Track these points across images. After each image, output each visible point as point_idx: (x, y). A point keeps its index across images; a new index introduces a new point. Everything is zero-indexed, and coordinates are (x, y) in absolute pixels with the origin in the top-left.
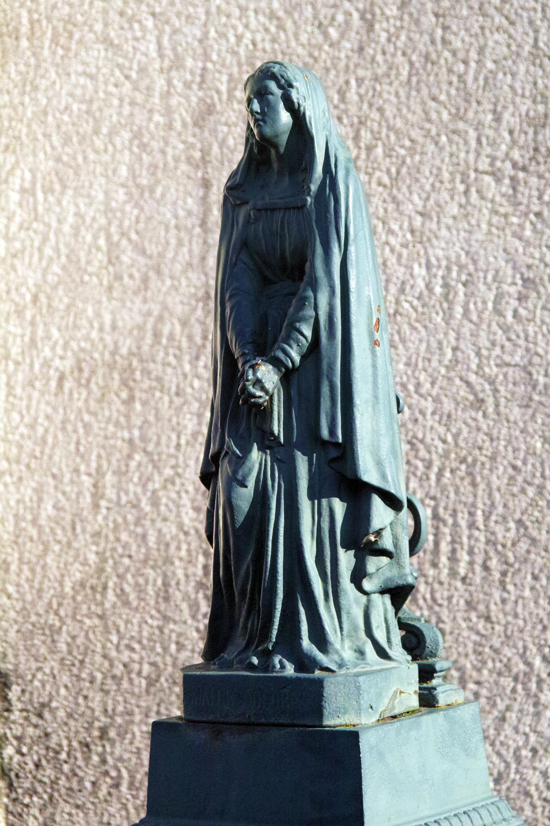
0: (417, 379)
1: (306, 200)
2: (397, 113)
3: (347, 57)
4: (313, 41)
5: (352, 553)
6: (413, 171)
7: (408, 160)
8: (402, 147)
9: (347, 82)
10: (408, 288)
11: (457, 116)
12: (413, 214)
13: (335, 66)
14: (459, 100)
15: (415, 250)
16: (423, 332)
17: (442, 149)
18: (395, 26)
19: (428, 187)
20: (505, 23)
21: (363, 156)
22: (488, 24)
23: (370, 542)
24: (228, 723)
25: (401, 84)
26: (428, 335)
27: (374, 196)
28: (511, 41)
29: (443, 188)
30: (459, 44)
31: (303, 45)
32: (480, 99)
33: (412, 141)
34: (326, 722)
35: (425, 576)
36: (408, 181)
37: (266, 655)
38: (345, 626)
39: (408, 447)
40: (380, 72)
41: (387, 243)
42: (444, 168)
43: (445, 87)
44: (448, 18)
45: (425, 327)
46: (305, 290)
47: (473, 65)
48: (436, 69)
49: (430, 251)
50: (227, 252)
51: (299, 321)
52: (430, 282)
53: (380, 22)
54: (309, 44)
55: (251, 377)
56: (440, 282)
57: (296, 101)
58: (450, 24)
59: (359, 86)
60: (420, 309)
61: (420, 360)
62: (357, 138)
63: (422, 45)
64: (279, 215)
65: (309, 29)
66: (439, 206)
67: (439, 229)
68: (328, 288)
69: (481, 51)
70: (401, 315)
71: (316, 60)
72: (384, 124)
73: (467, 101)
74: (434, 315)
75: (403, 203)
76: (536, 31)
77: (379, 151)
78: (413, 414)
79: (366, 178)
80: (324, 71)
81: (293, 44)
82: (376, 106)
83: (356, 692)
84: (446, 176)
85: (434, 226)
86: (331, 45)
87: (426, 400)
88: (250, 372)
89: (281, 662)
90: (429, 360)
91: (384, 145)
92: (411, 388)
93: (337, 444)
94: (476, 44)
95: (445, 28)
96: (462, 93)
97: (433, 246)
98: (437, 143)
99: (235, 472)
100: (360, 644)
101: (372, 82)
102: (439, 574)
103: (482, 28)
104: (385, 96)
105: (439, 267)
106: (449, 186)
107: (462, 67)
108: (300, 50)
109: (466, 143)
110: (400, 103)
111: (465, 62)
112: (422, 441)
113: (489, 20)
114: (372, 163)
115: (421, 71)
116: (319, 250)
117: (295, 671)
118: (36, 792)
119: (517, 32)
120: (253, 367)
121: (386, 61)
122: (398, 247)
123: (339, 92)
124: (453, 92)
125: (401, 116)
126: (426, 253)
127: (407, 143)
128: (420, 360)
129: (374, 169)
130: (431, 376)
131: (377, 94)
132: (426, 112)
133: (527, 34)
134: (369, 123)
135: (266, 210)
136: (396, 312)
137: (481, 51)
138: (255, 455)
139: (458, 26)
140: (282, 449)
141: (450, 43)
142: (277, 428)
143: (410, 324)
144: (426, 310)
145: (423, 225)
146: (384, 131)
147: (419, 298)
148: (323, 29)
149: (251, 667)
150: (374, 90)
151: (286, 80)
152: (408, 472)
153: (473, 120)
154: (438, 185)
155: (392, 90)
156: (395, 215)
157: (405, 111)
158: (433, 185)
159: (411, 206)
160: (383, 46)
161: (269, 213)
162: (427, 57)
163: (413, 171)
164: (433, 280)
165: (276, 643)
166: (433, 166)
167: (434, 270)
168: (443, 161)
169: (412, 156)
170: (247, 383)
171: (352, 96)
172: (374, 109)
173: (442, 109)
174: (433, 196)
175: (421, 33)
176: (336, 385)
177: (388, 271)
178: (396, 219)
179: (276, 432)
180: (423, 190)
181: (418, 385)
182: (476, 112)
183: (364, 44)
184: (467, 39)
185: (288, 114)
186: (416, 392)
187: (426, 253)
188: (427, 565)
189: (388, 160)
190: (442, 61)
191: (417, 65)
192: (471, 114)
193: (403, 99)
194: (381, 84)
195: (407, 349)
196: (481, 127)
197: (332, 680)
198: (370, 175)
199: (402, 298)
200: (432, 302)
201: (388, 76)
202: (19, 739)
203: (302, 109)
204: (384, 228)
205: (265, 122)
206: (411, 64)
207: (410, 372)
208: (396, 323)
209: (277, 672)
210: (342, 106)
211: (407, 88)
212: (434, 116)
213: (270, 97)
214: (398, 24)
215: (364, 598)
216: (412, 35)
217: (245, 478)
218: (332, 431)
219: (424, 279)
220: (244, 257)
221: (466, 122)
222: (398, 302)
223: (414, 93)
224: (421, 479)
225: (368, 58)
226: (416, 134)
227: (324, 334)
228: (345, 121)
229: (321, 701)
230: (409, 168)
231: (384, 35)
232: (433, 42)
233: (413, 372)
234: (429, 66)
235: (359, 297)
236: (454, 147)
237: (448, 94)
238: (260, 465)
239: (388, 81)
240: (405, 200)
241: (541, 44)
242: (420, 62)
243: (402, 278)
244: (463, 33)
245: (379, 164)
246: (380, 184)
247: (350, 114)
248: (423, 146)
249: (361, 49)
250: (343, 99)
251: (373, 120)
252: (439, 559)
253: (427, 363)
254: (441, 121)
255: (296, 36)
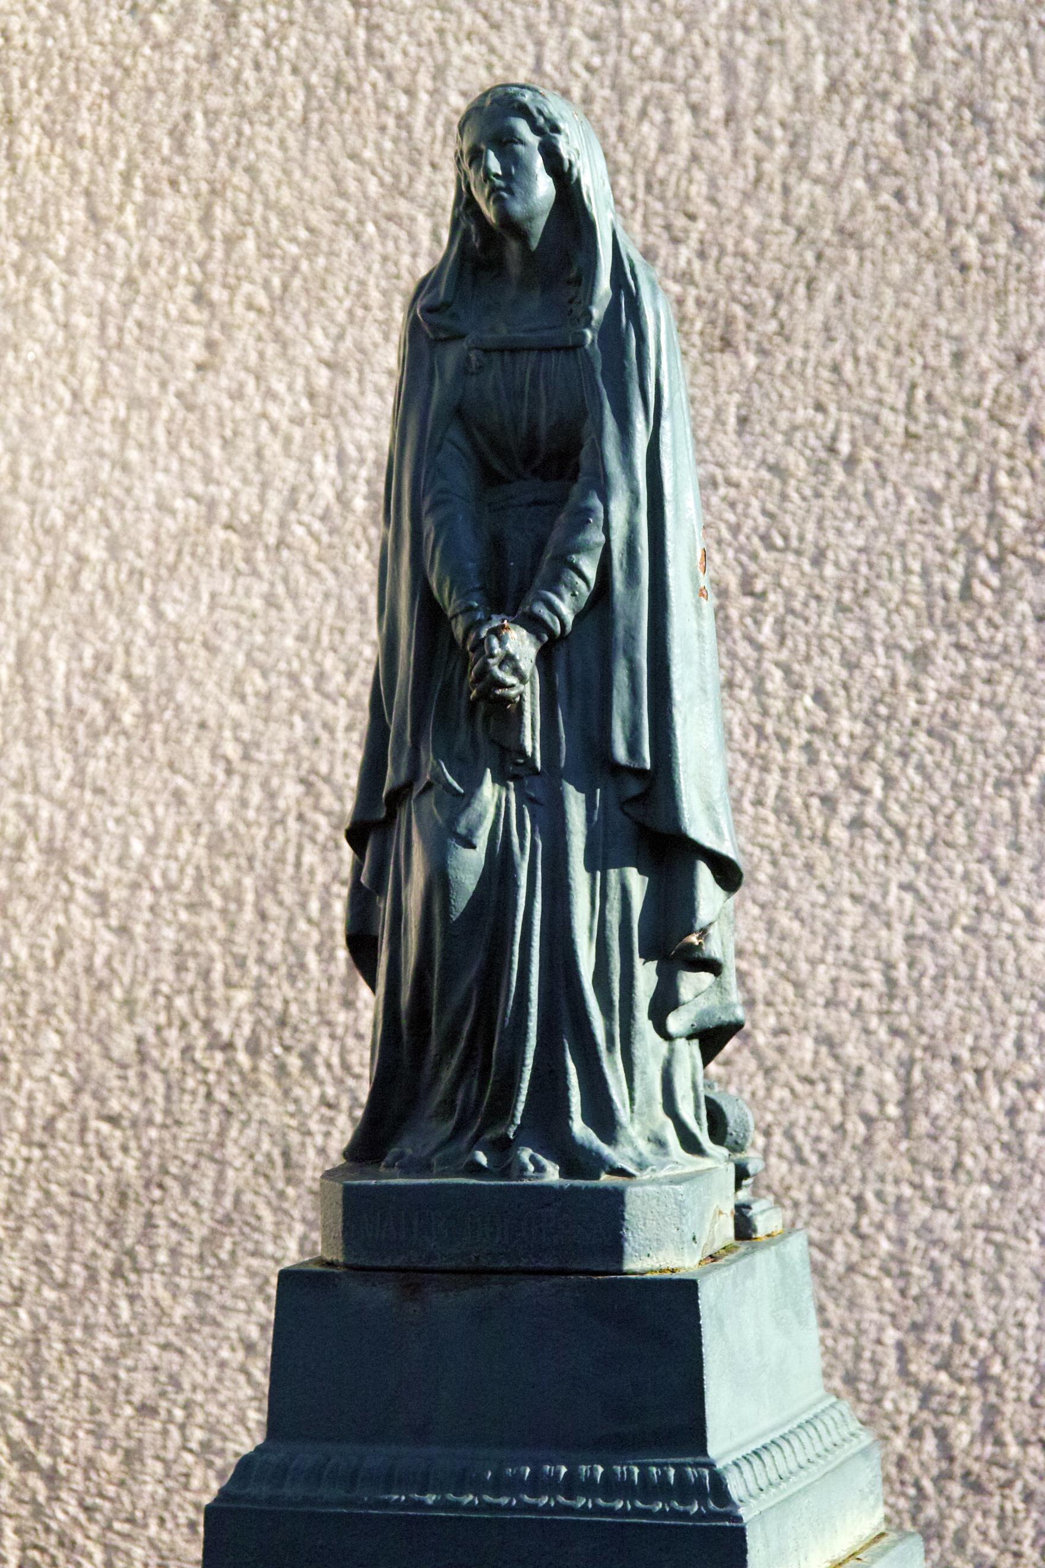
0: (319, 665)
1: (584, 336)
2: (284, 178)
3: (187, 70)
4: (123, 38)
5: (653, 965)
6: (314, 286)
7: (304, 265)
8: (293, 240)
9: (187, 117)
10: (303, 498)
11: (397, 190)
12: (313, 364)
13: (164, 86)
14: (398, 159)
15: (317, 429)
16: (331, 581)
17: (366, 248)
18: (278, 19)
19: (341, 317)
20: (483, 25)
21: (219, 253)
22: (451, 25)
23: (692, 945)
24: (433, 1271)
25: (289, 126)
26: (341, 587)
27: (239, 327)
28: (494, 59)
29: (370, 318)
30: (398, 59)
31: (101, 44)
32: (437, 160)
33: (310, 230)
35: (329, 1023)
36: (304, 304)
37: (503, 1148)
38: (638, 1095)
39: (300, 789)
40: (250, 100)
41: (264, 415)
42: (372, 282)
43: (372, 135)
44: (378, 10)
45: (335, 571)
46: (585, 496)
47: (424, 97)
48: (354, 101)
49: (346, 433)
50: (423, 423)
51: (578, 551)
52: (344, 489)
53: (250, 10)
54: (114, 43)
55: (497, 650)
56: (363, 489)
57: (565, 156)
58: (381, 20)
59: (210, 125)
60: (325, 538)
61: (325, 631)
62: (206, 220)
63: (329, 53)
64: (527, 362)
65: (114, 14)
66: (362, 351)
67: (362, 393)
68: (627, 494)
69: (439, 73)
70: (289, 547)
71: (127, 71)
72: (257, 196)
73: (414, 163)
74: (351, 549)
75: (294, 342)
76: (540, 43)
77: (249, 245)
78: (310, 728)
79: (225, 295)
80: (143, 94)
81: (83, 40)
82: (244, 162)
83: (677, 1213)
84: (375, 296)
85: (352, 387)
86: (156, 47)
87: (335, 703)
88: (495, 642)
89: (532, 1159)
90: (342, 632)
91: (258, 235)
92: (308, 681)
93: (641, 773)
94: (429, 61)
95: (372, 28)
96: (404, 148)
97: (349, 424)
98: (357, 237)
99: (452, 822)
100: (656, 1127)
101: (236, 119)
102: (356, 1020)
103: (441, 32)
104: (261, 145)
105: (362, 462)
106: (380, 316)
107: (404, 101)
108: (96, 52)
109: (412, 237)
110: (288, 160)
111: (410, 92)
112: (327, 779)
113: (453, 18)
114: (236, 267)
115: (328, 104)
116: (610, 425)
117: (564, 1174)
119: (504, 42)
120: (496, 632)
121: (261, 81)
122: (284, 424)
123: (171, 133)
124: (388, 145)
125: (290, 184)
126: (338, 435)
127: (303, 234)
128: (325, 631)
129: (239, 279)
130: (344, 660)
131: (244, 140)
132: (337, 180)
133: (522, 48)
134: (229, 194)
135: (501, 351)
136: (281, 543)
137: (439, 73)
138: (489, 791)
139: (396, 25)
140: (537, 780)
141: (382, 56)
142: (531, 742)
143: (306, 565)
144: (336, 540)
145: (332, 384)
146: (259, 210)
147: (323, 518)
148: (140, 16)
149: (476, 1169)
150: (240, 133)
151: (546, 120)
152: (300, 834)
153: (425, 198)
154: (359, 312)
155: (273, 135)
156: (281, 364)
157: (297, 175)
158: (350, 313)
159: (309, 350)
160: (256, 55)
161: (507, 357)
162: (338, 78)
163: (314, 286)
164: (351, 486)
165: (520, 1127)
166: (350, 278)
167: (353, 467)
168: (369, 270)
169: (310, 259)
170: (491, 661)
171: (197, 142)
172: (239, 169)
173: (367, 174)
174: (351, 332)
175: (327, 36)
176: (639, 667)
177: (266, 467)
178: (282, 373)
179: (529, 750)
180: (333, 321)
181: (321, 677)
182: (431, 184)
183: (219, 49)
184: (412, 50)
185: (550, 180)
186: (318, 689)
187: (338, 435)
188: (334, 1005)
189: (265, 263)
190: (367, 88)
191: (321, 92)
192: (420, 187)
193: (294, 151)
194: (251, 123)
195: (300, 611)
196: (438, 211)
197: (638, 1190)
198: (232, 289)
199: (293, 516)
200: (349, 526)
201: (266, 109)
203: (575, 171)
204: (258, 388)
205: (511, 192)
206: (309, 88)
207: (305, 653)
208: (280, 562)
209: (530, 1178)
210: (178, 160)
211: (301, 134)
212: (352, 186)
213: (520, 148)
214: (284, 15)
215: (663, 1046)
216: (310, 36)
217: (472, 831)
219: (333, 483)
220: (455, 433)
221: (412, 200)
222: (283, 524)
223: (314, 143)
224: (324, 848)
225: (228, 74)
226: (317, 217)
228: (184, 188)
229: (620, 1227)
230: (305, 280)
231: (257, 34)
232: (349, 52)
233: (312, 652)
234: (343, 95)
235: (677, 509)
236: (390, 244)
237: (379, 149)
238: (498, 807)
239: (265, 118)
240: (299, 339)
241: (548, 68)
242: (325, 87)
243: (291, 479)
244: (404, 38)
245: (250, 270)
246: (250, 306)
247: (193, 174)
248: (332, 241)
249: (214, 57)
250: (180, 147)
251: (236, 188)
252: (357, 992)
253: (337, 637)
254: (366, 197)
255: (88, 24)
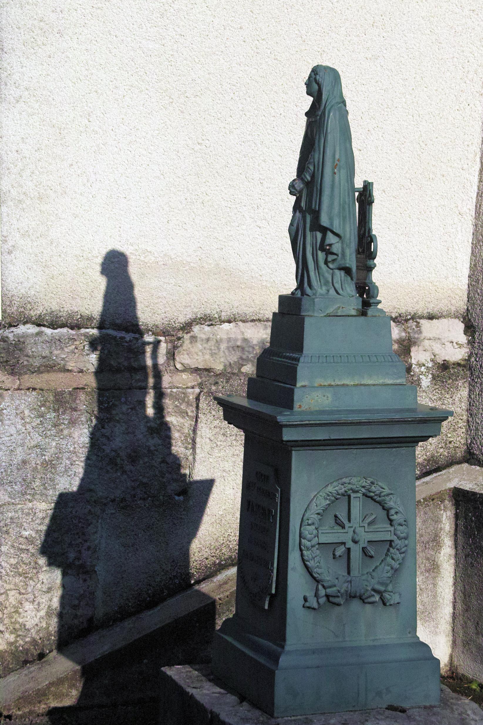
34: (302, 314)
38: (322, 281)
118: (479, 377)
202: (476, 354)
215: (331, 271)
218: (315, 206)
227: (316, 169)
